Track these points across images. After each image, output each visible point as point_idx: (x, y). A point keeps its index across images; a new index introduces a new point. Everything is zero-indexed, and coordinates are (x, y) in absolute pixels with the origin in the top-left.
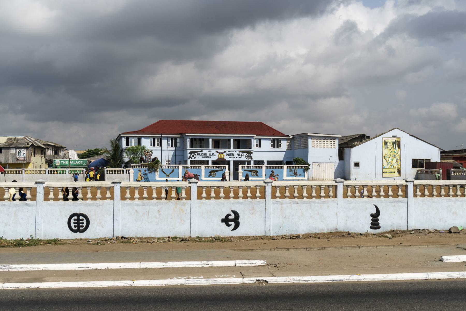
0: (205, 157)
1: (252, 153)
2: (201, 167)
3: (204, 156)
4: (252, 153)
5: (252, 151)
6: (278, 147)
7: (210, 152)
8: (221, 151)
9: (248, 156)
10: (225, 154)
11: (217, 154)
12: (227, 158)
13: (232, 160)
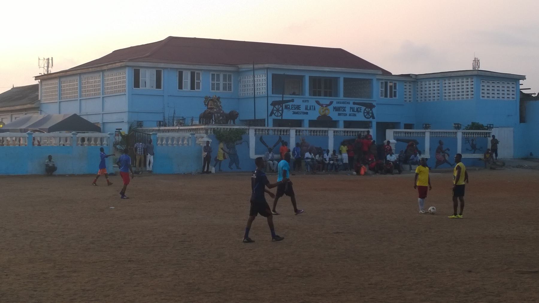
0: (297, 113)
1: (374, 106)
2: (456, 132)
3: (296, 111)
4: (374, 106)
5: (374, 103)
6: (391, 96)
7: (306, 104)
8: (325, 100)
9: (368, 113)
10: (331, 108)
11: (318, 107)
12: (334, 115)
13: (341, 119)
